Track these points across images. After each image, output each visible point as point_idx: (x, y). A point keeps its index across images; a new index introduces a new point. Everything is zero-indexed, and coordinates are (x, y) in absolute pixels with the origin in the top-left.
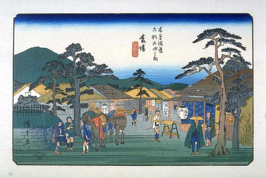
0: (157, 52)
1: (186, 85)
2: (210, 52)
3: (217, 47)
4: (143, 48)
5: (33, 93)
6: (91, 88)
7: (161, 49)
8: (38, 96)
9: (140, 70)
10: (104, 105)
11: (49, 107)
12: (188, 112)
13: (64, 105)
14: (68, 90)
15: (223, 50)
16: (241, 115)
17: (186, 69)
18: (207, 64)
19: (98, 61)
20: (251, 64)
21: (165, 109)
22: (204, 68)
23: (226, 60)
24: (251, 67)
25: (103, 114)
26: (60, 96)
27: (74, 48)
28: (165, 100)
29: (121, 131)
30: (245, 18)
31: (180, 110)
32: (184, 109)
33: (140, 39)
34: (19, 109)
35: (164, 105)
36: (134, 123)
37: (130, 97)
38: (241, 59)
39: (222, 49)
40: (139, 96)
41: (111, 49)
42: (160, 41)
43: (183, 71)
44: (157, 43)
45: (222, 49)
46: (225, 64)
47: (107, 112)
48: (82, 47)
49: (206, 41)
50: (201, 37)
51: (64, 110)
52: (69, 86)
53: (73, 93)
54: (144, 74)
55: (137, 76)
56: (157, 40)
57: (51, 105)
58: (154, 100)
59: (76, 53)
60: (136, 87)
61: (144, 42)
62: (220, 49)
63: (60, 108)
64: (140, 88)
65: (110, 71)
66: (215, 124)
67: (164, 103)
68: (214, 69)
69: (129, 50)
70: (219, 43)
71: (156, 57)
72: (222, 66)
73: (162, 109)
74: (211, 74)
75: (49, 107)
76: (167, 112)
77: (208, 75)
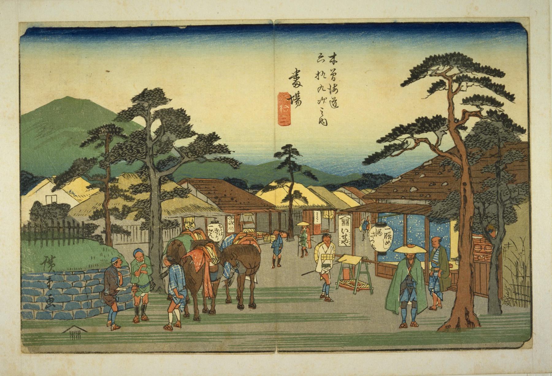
0: (327, 106)
1: (387, 178)
2: (437, 106)
3: (451, 94)
4: (298, 99)
5: (62, 197)
6: (185, 186)
7: (335, 100)
8: (73, 203)
9: (289, 146)
10: (212, 223)
11: (96, 227)
12: (392, 236)
13: (128, 222)
14: (136, 189)
15: (466, 101)
16: (505, 242)
17: (387, 144)
18: (432, 133)
19: (200, 126)
20: (525, 130)
21: (344, 229)
22: (426, 140)
23: (471, 122)
24: (523, 138)
25: (211, 241)
26: (118, 203)
27: (151, 97)
28: (342, 212)
29: (247, 278)
30: (512, 28)
31: (375, 232)
32: (384, 230)
33: (290, 78)
34: (33, 230)
35: (340, 222)
36: (276, 262)
37: (270, 207)
38: (504, 118)
39: (463, 100)
40: (287, 203)
41: (233, 104)
42: (332, 83)
43: (380, 148)
44: (326, 87)
45: (463, 100)
46: (469, 130)
47: (220, 238)
48: (167, 96)
49: (427, 81)
50: (417, 74)
51: (128, 233)
52: (136, 181)
53: (145, 196)
54: (297, 153)
55: (284, 158)
56: (326, 82)
57: (101, 223)
58: (319, 212)
59: (153, 111)
60: (281, 182)
61: (300, 85)
62: (458, 99)
63: (118, 230)
64: (289, 184)
65: (224, 149)
66: (450, 262)
67: (340, 217)
68: (447, 143)
69: (272, 107)
70: (455, 86)
71: (323, 118)
72: (464, 134)
73: (336, 230)
74: (442, 154)
75: (96, 227)
76: (116, 140)
77: (434, 155)
